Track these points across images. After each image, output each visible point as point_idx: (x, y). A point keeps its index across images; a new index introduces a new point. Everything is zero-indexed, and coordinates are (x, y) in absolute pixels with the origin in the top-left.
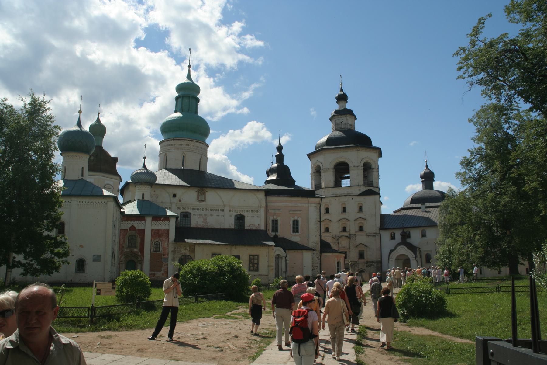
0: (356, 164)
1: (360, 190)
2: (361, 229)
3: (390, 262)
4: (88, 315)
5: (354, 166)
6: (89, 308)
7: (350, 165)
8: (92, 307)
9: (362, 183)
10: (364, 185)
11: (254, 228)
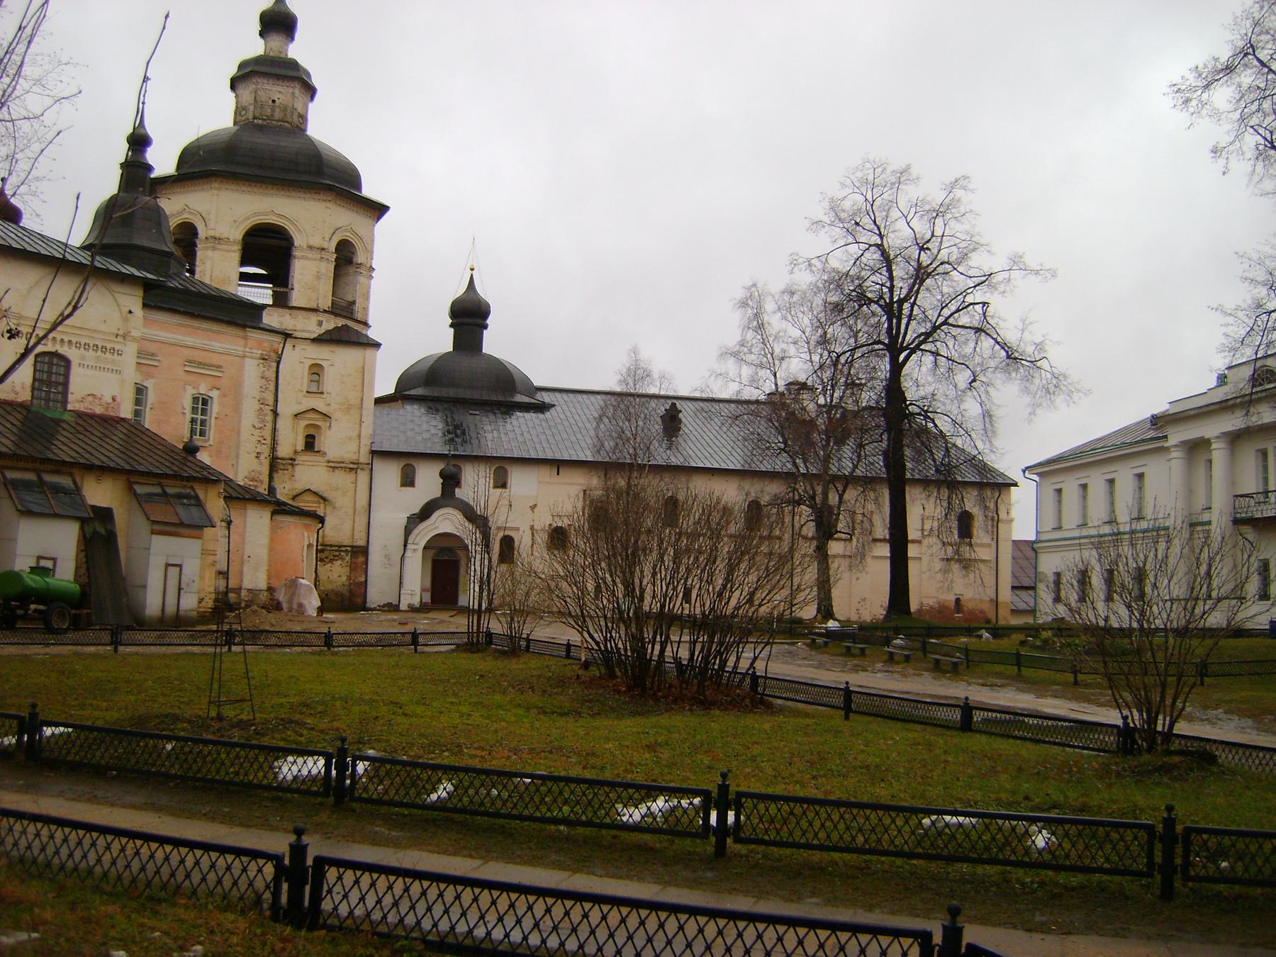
0: (316, 241)
1: (320, 323)
2: (310, 443)
3: (409, 554)
4: (1151, 863)
5: (311, 247)
6: (1150, 829)
7: (299, 241)
8: (1170, 823)
9: (326, 303)
10: (335, 311)
11: (99, 410)
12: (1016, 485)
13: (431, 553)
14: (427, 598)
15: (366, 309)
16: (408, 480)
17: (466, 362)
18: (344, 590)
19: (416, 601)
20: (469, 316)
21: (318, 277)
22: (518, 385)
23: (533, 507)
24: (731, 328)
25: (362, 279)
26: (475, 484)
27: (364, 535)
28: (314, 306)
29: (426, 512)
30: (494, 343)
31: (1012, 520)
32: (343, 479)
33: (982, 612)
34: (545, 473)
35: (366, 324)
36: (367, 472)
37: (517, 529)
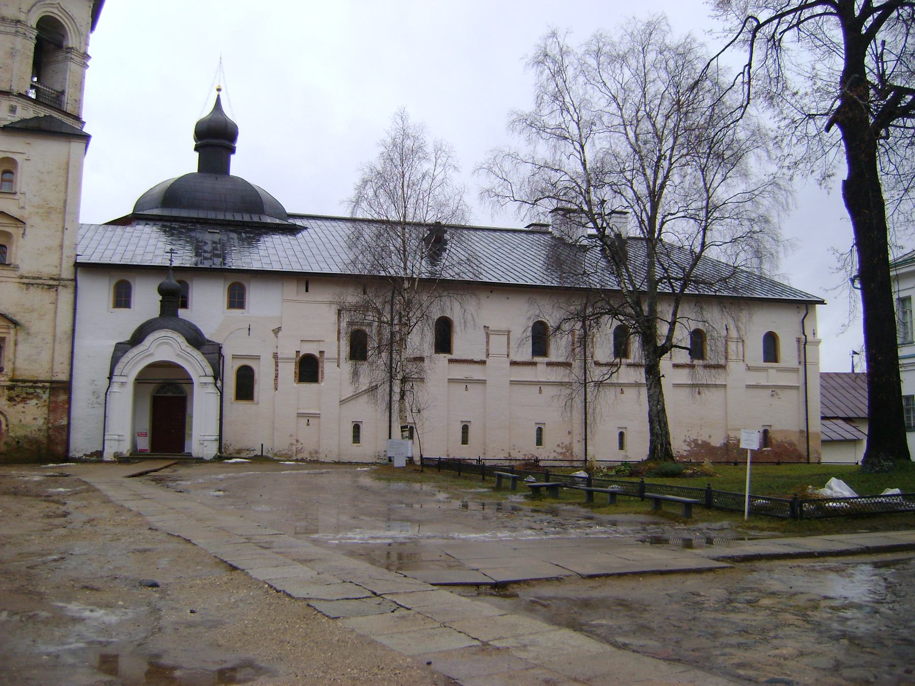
3: (115, 388)
12: (822, 302)
13: (150, 389)
14: (144, 444)
15: (78, 102)
16: (122, 299)
17: (210, 183)
18: (41, 436)
19: (125, 448)
20: (216, 138)
21: (12, 53)
22: (266, 208)
23: (277, 331)
24: (522, 90)
25: (73, 66)
26: (207, 306)
27: (66, 367)
28: (7, 89)
29: (138, 337)
30: (241, 166)
31: (819, 342)
32: (39, 298)
33: (791, 444)
34: (291, 290)
35: (78, 118)
36: (71, 290)
37: (257, 358)
